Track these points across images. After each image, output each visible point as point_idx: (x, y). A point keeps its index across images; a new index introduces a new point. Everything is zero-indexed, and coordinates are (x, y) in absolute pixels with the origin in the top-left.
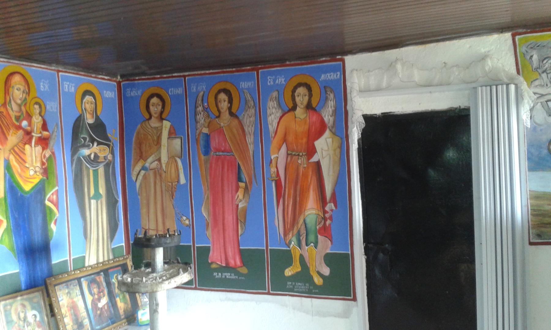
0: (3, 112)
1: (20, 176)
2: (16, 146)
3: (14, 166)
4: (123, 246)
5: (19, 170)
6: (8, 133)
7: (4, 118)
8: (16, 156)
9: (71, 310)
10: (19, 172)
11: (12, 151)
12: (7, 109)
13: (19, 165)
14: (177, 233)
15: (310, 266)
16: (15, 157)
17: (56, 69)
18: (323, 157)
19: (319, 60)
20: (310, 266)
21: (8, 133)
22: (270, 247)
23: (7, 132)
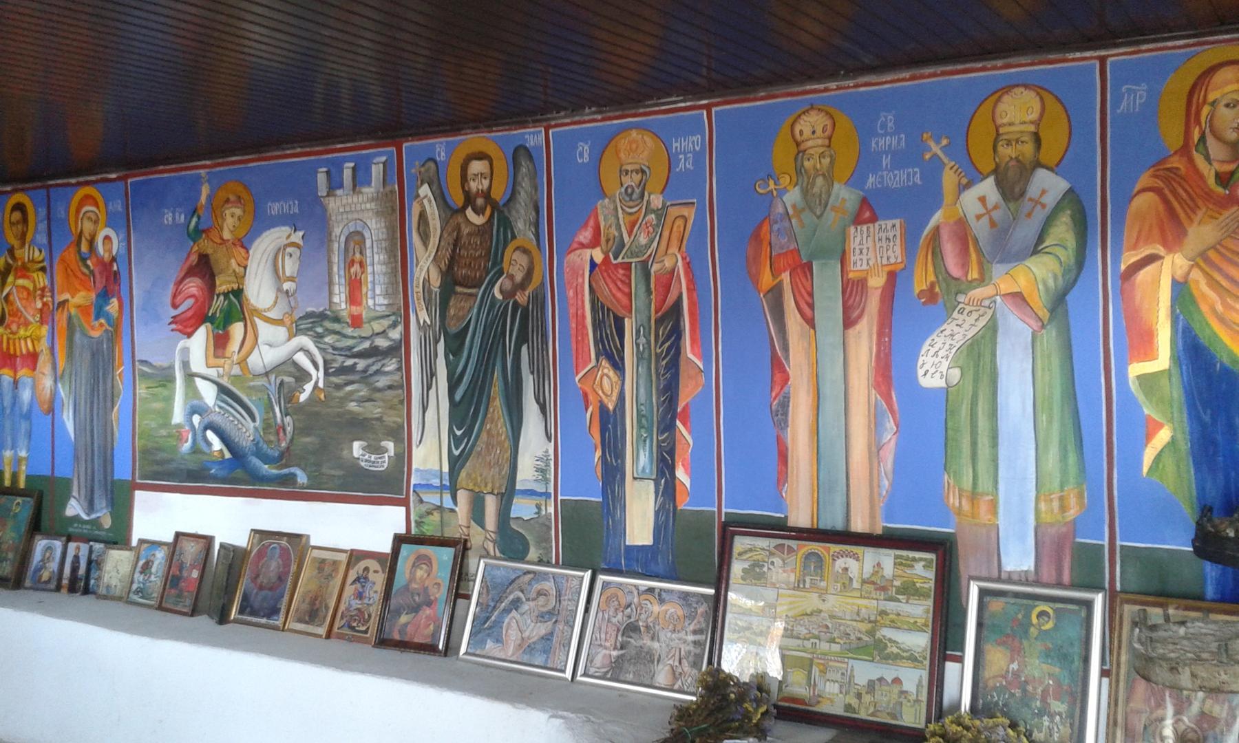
0: (1177, 169)
1: (1222, 320)
2: (1214, 247)
3: (1204, 295)
4: (714, 512)
5: (1219, 308)
6: (1189, 217)
7: (1182, 181)
8: (1208, 269)
9: (1149, 700)
10: (1217, 313)
11: (1199, 260)
12: (1191, 161)
13: (1221, 297)
14: (667, 489)
15: (1215, 622)
16: (1206, 274)
17: (337, 286)
18: (53, 415)
19: (646, 103)
20: (1215, 622)
21: (1189, 217)
22: (1122, 540)
23: (1187, 214)
